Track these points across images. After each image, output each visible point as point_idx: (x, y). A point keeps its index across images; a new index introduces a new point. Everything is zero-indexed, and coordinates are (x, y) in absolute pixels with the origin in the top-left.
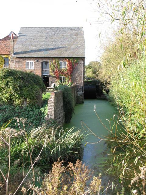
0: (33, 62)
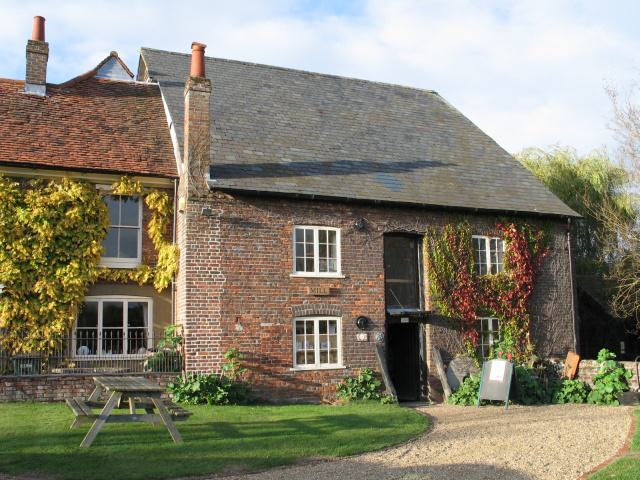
0: (338, 231)
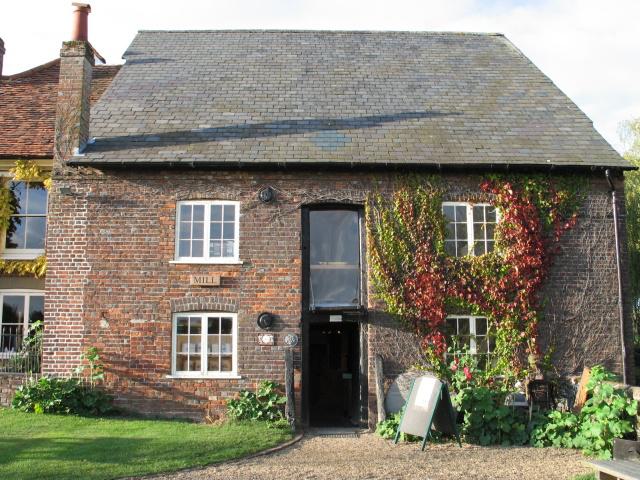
0: (237, 205)
